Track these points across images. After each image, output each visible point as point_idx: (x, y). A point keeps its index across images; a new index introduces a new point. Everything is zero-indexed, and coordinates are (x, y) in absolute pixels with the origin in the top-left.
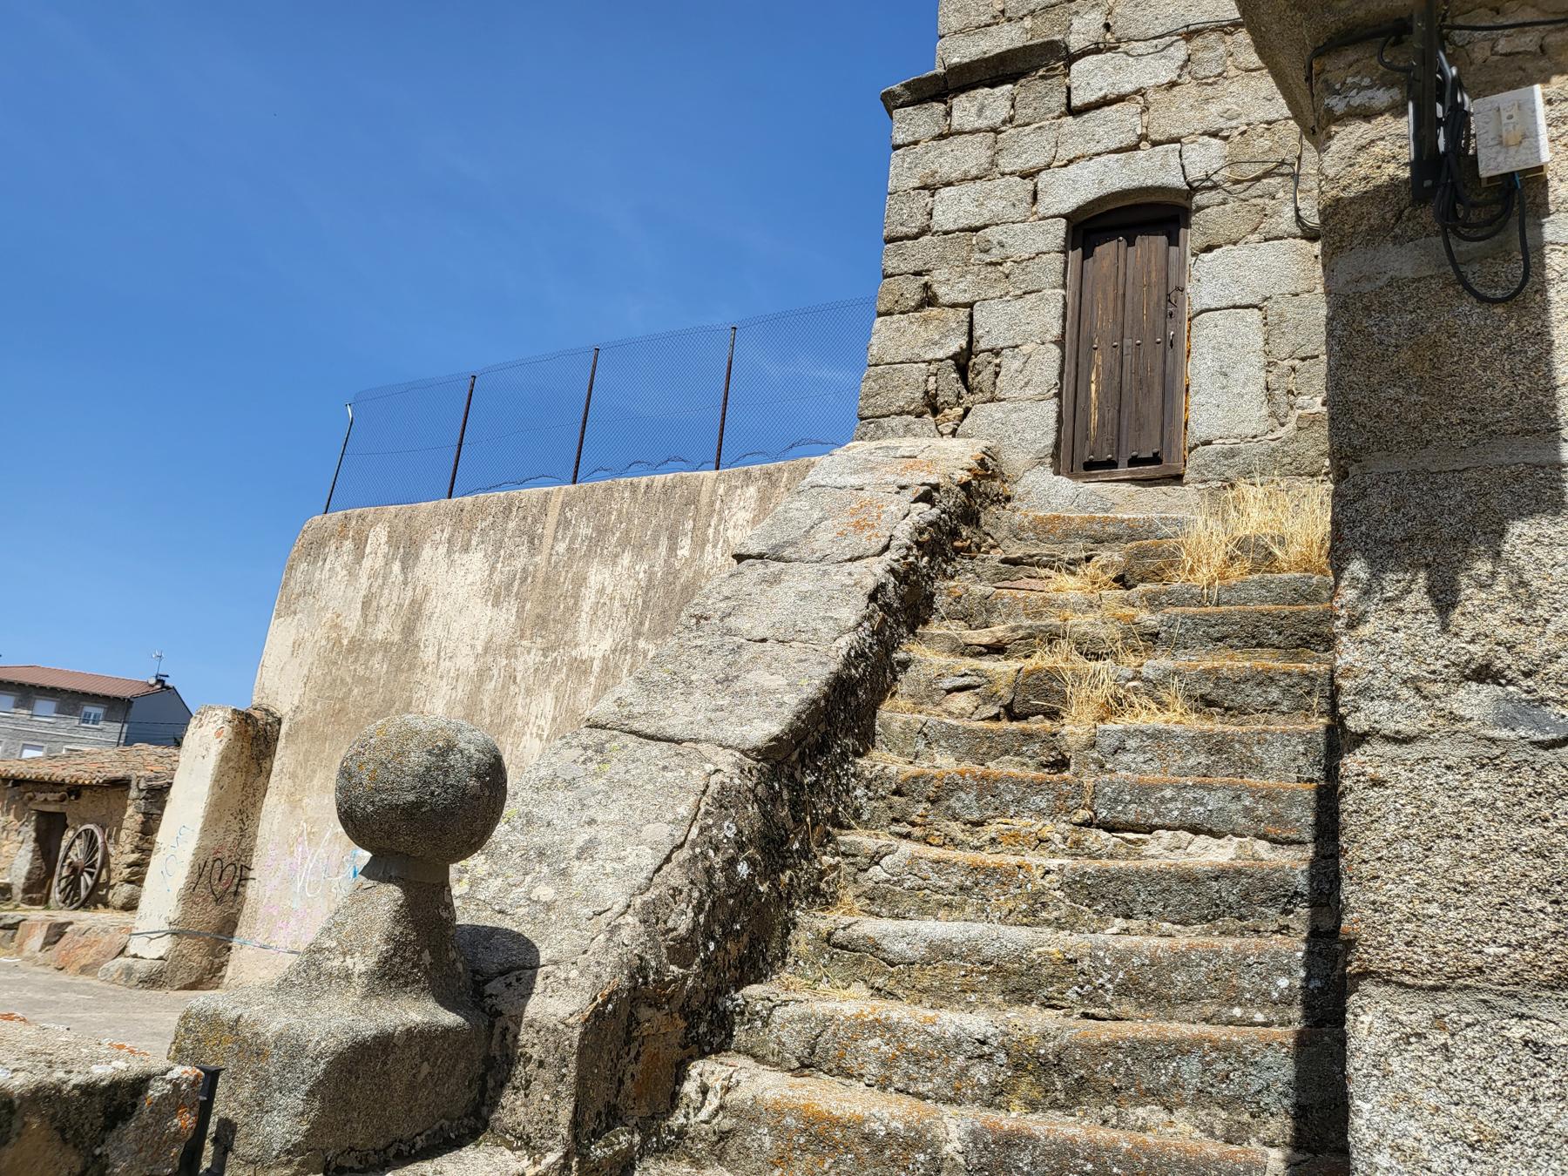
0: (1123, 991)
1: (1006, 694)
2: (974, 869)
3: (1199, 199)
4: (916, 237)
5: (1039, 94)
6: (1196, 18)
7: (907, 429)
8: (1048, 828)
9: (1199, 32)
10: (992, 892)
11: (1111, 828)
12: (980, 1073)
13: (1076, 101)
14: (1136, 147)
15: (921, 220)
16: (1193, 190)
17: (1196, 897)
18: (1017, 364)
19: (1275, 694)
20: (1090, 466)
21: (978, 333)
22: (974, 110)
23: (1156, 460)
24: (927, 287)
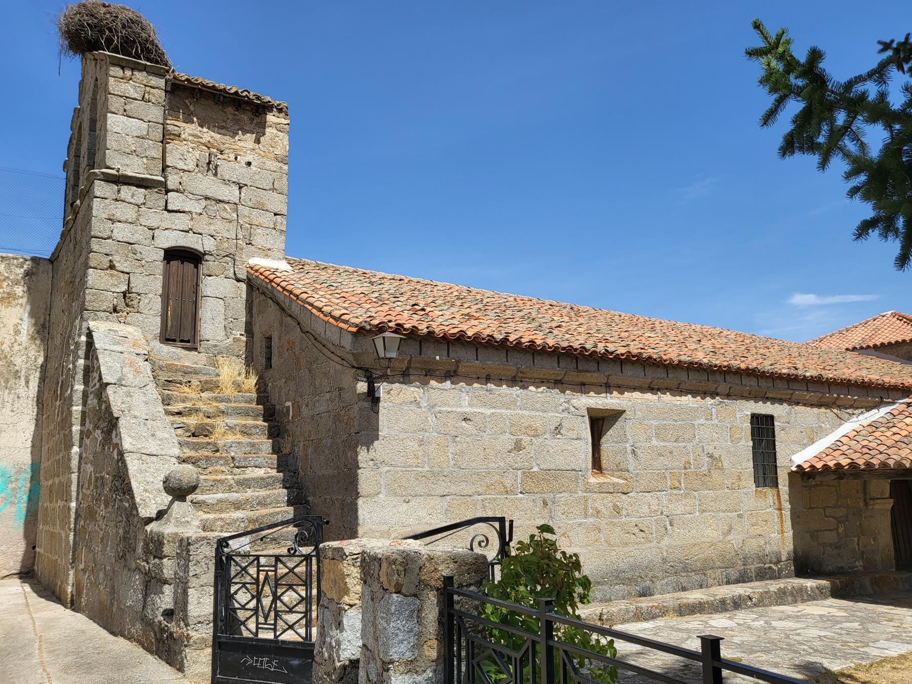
0: (258, 504)
1: (193, 430)
2: (214, 481)
4: (105, 239)
5: (154, 197)
6: (210, 195)
7: (107, 318)
8: (223, 468)
9: (209, 199)
11: (238, 467)
13: (169, 208)
14: (187, 232)
15: (108, 233)
16: (205, 254)
17: (262, 483)
18: (147, 301)
20: (167, 340)
21: (132, 285)
22: (130, 194)
23: (188, 341)
24: (111, 261)
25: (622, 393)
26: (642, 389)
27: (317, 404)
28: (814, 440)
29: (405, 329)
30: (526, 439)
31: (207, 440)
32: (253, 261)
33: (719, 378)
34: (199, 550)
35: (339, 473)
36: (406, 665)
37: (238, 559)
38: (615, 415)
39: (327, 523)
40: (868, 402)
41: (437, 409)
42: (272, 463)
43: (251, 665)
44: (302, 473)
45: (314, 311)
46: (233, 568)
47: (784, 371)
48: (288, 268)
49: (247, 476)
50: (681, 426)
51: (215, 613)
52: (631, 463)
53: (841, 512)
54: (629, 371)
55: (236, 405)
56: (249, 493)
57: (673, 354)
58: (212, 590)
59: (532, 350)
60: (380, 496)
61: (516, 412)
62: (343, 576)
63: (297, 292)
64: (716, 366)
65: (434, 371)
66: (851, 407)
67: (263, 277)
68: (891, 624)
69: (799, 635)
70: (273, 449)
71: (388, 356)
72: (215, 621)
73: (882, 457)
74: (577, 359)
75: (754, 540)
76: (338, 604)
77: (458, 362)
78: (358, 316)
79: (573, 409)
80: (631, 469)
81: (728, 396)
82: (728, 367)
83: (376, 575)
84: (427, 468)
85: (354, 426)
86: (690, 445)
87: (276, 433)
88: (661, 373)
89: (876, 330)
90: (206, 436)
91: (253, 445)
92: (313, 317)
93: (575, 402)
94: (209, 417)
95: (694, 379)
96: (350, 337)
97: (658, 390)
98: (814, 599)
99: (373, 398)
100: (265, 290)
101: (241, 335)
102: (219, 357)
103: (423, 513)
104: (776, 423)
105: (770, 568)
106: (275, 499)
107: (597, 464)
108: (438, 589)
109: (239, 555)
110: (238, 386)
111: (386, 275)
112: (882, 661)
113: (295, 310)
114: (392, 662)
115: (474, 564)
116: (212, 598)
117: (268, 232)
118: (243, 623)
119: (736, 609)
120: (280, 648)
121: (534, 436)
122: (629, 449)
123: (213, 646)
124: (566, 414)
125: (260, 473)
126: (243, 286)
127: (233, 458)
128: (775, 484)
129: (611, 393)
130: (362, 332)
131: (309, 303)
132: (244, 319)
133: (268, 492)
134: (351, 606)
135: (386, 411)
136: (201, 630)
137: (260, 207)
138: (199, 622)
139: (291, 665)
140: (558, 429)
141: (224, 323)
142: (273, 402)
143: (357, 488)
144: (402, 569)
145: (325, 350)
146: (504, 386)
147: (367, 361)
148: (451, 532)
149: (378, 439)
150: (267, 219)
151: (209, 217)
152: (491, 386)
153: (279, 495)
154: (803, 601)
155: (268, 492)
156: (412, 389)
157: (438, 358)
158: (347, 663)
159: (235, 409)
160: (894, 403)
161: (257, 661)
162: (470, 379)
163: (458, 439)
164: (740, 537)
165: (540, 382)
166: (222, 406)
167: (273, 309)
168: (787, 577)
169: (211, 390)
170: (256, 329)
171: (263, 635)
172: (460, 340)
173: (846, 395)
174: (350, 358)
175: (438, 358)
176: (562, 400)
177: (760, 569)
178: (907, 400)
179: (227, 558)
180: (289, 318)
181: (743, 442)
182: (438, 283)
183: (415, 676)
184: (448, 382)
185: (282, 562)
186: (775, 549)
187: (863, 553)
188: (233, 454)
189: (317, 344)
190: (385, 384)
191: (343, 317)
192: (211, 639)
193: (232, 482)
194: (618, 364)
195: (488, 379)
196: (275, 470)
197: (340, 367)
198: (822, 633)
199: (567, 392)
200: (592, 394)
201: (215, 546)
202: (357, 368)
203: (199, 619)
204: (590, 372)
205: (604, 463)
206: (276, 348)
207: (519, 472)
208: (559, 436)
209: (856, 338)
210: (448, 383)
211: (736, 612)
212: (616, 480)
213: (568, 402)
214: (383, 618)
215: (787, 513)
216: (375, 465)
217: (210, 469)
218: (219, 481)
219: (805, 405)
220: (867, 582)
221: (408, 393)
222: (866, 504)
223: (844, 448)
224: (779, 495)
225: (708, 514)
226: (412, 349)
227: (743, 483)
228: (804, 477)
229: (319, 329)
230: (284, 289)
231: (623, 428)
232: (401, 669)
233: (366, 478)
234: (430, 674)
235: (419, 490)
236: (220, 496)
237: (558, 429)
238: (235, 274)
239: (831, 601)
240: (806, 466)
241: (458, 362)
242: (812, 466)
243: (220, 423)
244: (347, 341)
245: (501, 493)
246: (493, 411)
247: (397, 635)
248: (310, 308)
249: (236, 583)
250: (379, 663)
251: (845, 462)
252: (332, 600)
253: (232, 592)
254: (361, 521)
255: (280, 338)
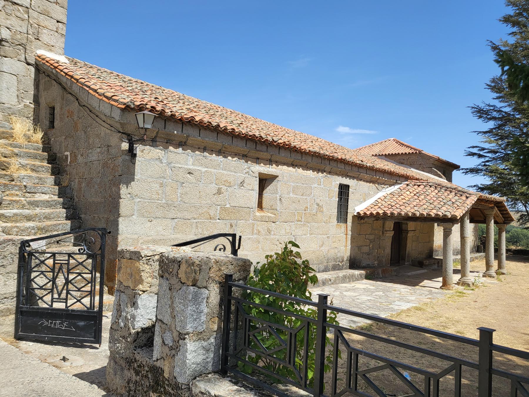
0: (44, 218)
2: (11, 201)
3: (3, 43)
8: (17, 193)
10: (15, 204)
11: (29, 193)
12: (33, 231)
17: (48, 204)
19: (44, 169)
25: (278, 166)
26: (288, 165)
27: (90, 155)
28: (367, 199)
29: (156, 111)
30: (224, 188)
31: (4, 172)
32: (40, 52)
33: (327, 162)
34: (6, 249)
35: (105, 201)
36: (198, 335)
37: (37, 255)
38: (273, 178)
39: (110, 233)
40: (391, 182)
41: (173, 165)
42: (55, 192)
43: (47, 326)
44: (76, 199)
45: (91, 91)
46: (33, 261)
47: (358, 162)
48: (67, 62)
49: (36, 199)
50: (306, 187)
51: (19, 291)
52: (279, 206)
53: (372, 237)
54: (283, 153)
55: (27, 150)
56: (38, 210)
57: (306, 146)
58: (16, 276)
59: (233, 135)
60: (134, 217)
61: (219, 171)
62: (139, 271)
63: (77, 77)
64: (327, 155)
65: (172, 140)
66: (383, 184)
67: (49, 64)
68: (396, 292)
69: (358, 299)
70: (55, 182)
71: (146, 127)
72: (18, 297)
73: (398, 210)
74: (256, 143)
75: (333, 250)
76: (133, 290)
77: (188, 136)
78: (125, 98)
79: (251, 173)
80: (278, 209)
81: (330, 173)
82: (333, 156)
83: (175, 272)
84: (164, 201)
85: (118, 171)
86: (308, 198)
87: (57, 172)
88: (299, 156)
89: (386, 147)
90: (4, 170)
91: (40, 179)
92: (90, 96)
93: (252, 168)
94: (5, 157)
95: (315, 162)
96: (119, 111)
97: (296, 166)
98: (358, 280)
99: (132, 153)
100: (50, 74)
101: (30, 103)
102: (12, 117)
103: (160, 229)
104: (350, 190)
105: (338, 264)
106: (57, 215)
107: (260, 205)
108: (220, 283)
109: (37, 252)
110: (28, 138)
111: (132, 79)
112: (401, 312)
113: (75, 89)
114: (188, 334)
115: (243, 266)
116: (16, 281)
117: (52, 33)
118: (41, 298)
119: (323, 285)
120: (70, 314)
121: (228, 186)
122: (278, 198)
123: (17, 313)
124: (247, 175)
125: (46, 197)
126: (32, 69)
127: (25, 186)
128: (346, 221)
129: (272, 165)
130: (127, 109)
131: (86, 86)
132: (33, 93)
133: (52, 211)
134: (144, 292)
135: (140, 163)
136: (6, 303)
137: (45, 13)
138: (5, 298)
139: (78, 326)
140: (242, 183)
141: (17, 93)
142: (55, 151)
143: (119, 211)
144: (198, 269)
145: (98, 119)
146: (214, 155)
147: (130, 129)
148: (202, 242)
149: (134, 181)
150: (52, 24)
151: (7, 14)
152: (206, 154)
153: (60, 213)
154: (353, 281)
155: (52, 211)
156: (157, 150)
157: (175, 132)
158: (140, 330)
159: (26, 153)
160: (401, 184)
161: (51, 323)
162: (194, 148)
163: (184, 185)
164: (327, 248)
165: (235, 155)
166: (16, 150)
167: (56, 90)
168: (346, 269)
169: (7, 138)
170: (42, 101)
171: (56, 305)
172: (190, 122)
173: (382, 178)
174: (118, 126)
175: (175, 132)
176: (246, 167)
177: (334, 265)
178: (406, 183)
179: (28, 255)
180: (69, 95)
181: (334, 199)
182: (165, 89)
183: (203, 342)
184: (181, 149)
185: (72, 257)
186: (342, 255)
187: (378, 257)
188: (25, 184)
189: (92, 115)
190: (141, 145)
191: (114, 98)
192: (14, 309)
193: (25, 202)
194: (278, 149)
195: (205, 149)
196: (57, 196)
197: (109, 131)
198: (369, 298)
199: (249, 162)
200: (262, 164)
201: (19, 245)
202: (122, 133)
203: (5, 296)
204: (262, 151)
205: (264, 206)
206: (58, 115)
207: (219, 207)
208: (242, 188)
209: (377, 150)
210: (180, 150)
211: (324, 287)
212: (270, 215)
213: (249, 168)
214: (180, 303)
215: (349, 237)
216: (131, 197)
217: (7, 193)
218: (14, 201)
219: (364, 181)
220: (380, 271)
221: (155, 153)
222: (383, 233)
223: (380, 205)
224: (347, 227)
225: (313, 236)
226: (160, 124)
227: (331, 220)
228: (359, 218)
229: (95, 104)
230: (66, 74)
231: (276, 185)
232: (194, 338)
233: (125, 206)
234: (212, 340)
235: (158, 214)
236: (15, 211)
237: (242, 183)
238: (26, 59)
239: (365, 281)
240: (362, 213)
241: (188, 136)
242: (365, 213)
243: (15, 162)
244: (117, 115)
245: (207, 219)
246: (206, 169)
247: (192, 315)
248: (88, 89)
249: (35, 271)
250: (175, 334)
251: (381, 212)
252: (128, 287)
253: (32, 277)
254: (120, 232)
255: (61, 108)
